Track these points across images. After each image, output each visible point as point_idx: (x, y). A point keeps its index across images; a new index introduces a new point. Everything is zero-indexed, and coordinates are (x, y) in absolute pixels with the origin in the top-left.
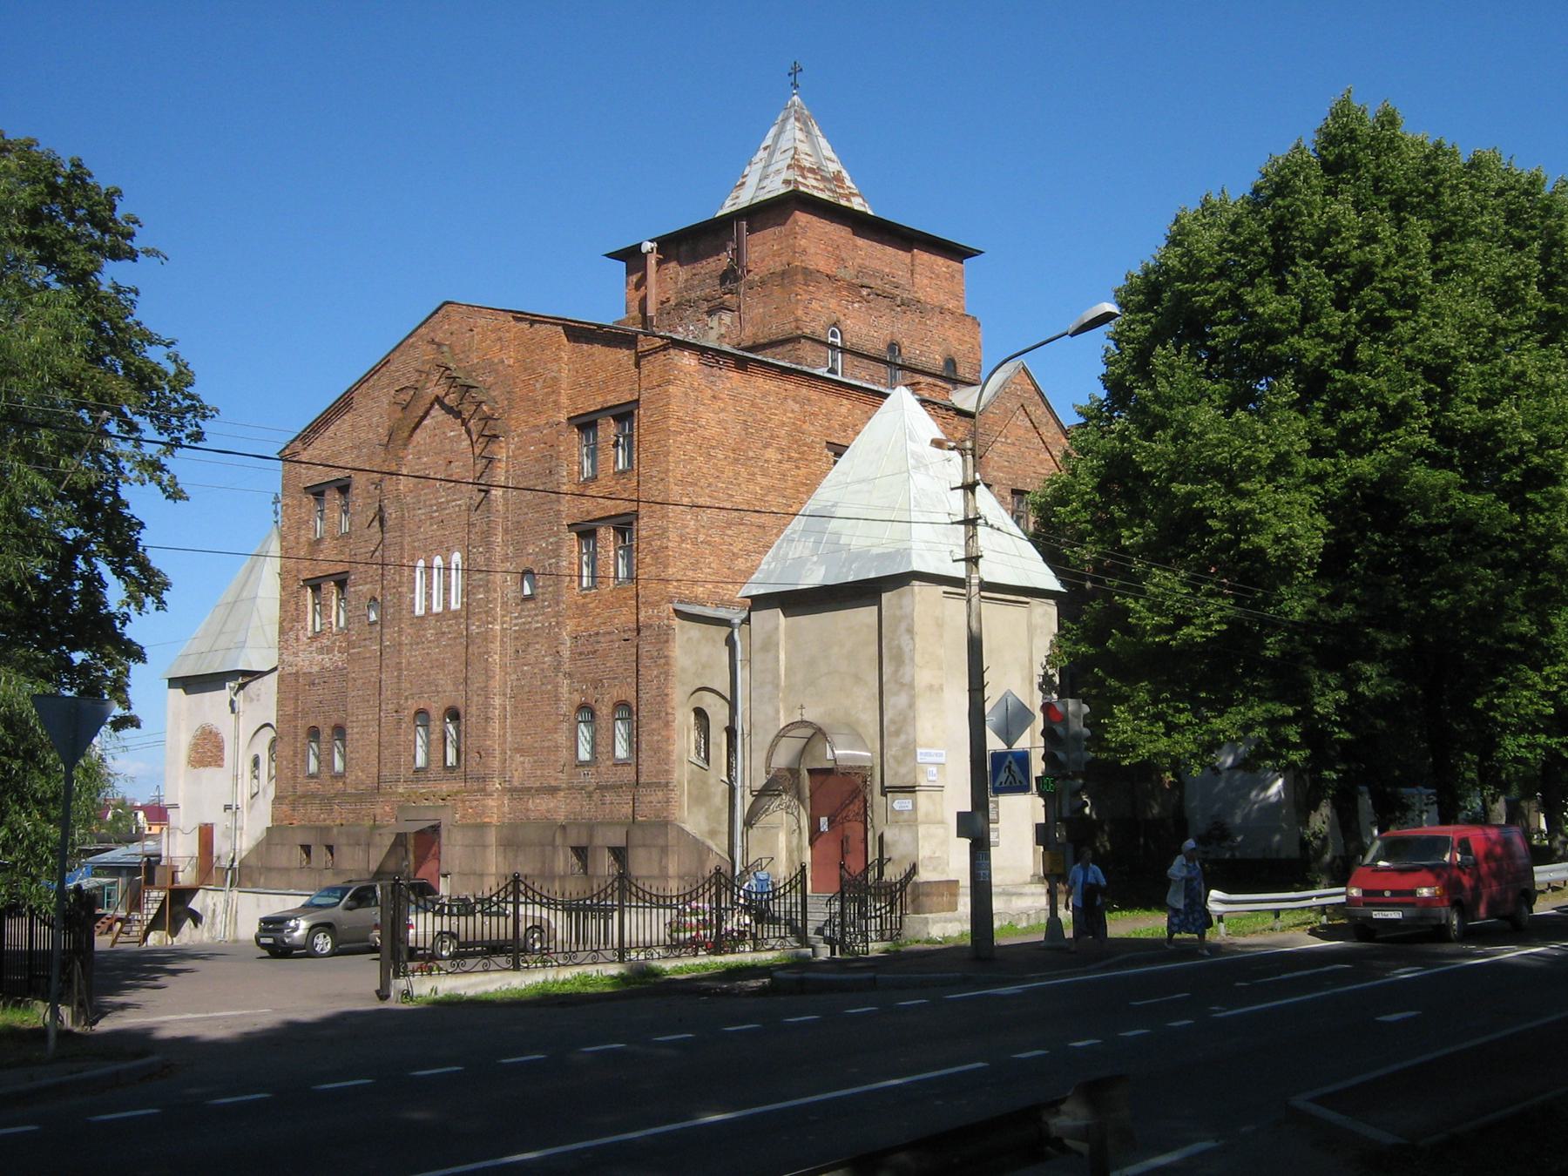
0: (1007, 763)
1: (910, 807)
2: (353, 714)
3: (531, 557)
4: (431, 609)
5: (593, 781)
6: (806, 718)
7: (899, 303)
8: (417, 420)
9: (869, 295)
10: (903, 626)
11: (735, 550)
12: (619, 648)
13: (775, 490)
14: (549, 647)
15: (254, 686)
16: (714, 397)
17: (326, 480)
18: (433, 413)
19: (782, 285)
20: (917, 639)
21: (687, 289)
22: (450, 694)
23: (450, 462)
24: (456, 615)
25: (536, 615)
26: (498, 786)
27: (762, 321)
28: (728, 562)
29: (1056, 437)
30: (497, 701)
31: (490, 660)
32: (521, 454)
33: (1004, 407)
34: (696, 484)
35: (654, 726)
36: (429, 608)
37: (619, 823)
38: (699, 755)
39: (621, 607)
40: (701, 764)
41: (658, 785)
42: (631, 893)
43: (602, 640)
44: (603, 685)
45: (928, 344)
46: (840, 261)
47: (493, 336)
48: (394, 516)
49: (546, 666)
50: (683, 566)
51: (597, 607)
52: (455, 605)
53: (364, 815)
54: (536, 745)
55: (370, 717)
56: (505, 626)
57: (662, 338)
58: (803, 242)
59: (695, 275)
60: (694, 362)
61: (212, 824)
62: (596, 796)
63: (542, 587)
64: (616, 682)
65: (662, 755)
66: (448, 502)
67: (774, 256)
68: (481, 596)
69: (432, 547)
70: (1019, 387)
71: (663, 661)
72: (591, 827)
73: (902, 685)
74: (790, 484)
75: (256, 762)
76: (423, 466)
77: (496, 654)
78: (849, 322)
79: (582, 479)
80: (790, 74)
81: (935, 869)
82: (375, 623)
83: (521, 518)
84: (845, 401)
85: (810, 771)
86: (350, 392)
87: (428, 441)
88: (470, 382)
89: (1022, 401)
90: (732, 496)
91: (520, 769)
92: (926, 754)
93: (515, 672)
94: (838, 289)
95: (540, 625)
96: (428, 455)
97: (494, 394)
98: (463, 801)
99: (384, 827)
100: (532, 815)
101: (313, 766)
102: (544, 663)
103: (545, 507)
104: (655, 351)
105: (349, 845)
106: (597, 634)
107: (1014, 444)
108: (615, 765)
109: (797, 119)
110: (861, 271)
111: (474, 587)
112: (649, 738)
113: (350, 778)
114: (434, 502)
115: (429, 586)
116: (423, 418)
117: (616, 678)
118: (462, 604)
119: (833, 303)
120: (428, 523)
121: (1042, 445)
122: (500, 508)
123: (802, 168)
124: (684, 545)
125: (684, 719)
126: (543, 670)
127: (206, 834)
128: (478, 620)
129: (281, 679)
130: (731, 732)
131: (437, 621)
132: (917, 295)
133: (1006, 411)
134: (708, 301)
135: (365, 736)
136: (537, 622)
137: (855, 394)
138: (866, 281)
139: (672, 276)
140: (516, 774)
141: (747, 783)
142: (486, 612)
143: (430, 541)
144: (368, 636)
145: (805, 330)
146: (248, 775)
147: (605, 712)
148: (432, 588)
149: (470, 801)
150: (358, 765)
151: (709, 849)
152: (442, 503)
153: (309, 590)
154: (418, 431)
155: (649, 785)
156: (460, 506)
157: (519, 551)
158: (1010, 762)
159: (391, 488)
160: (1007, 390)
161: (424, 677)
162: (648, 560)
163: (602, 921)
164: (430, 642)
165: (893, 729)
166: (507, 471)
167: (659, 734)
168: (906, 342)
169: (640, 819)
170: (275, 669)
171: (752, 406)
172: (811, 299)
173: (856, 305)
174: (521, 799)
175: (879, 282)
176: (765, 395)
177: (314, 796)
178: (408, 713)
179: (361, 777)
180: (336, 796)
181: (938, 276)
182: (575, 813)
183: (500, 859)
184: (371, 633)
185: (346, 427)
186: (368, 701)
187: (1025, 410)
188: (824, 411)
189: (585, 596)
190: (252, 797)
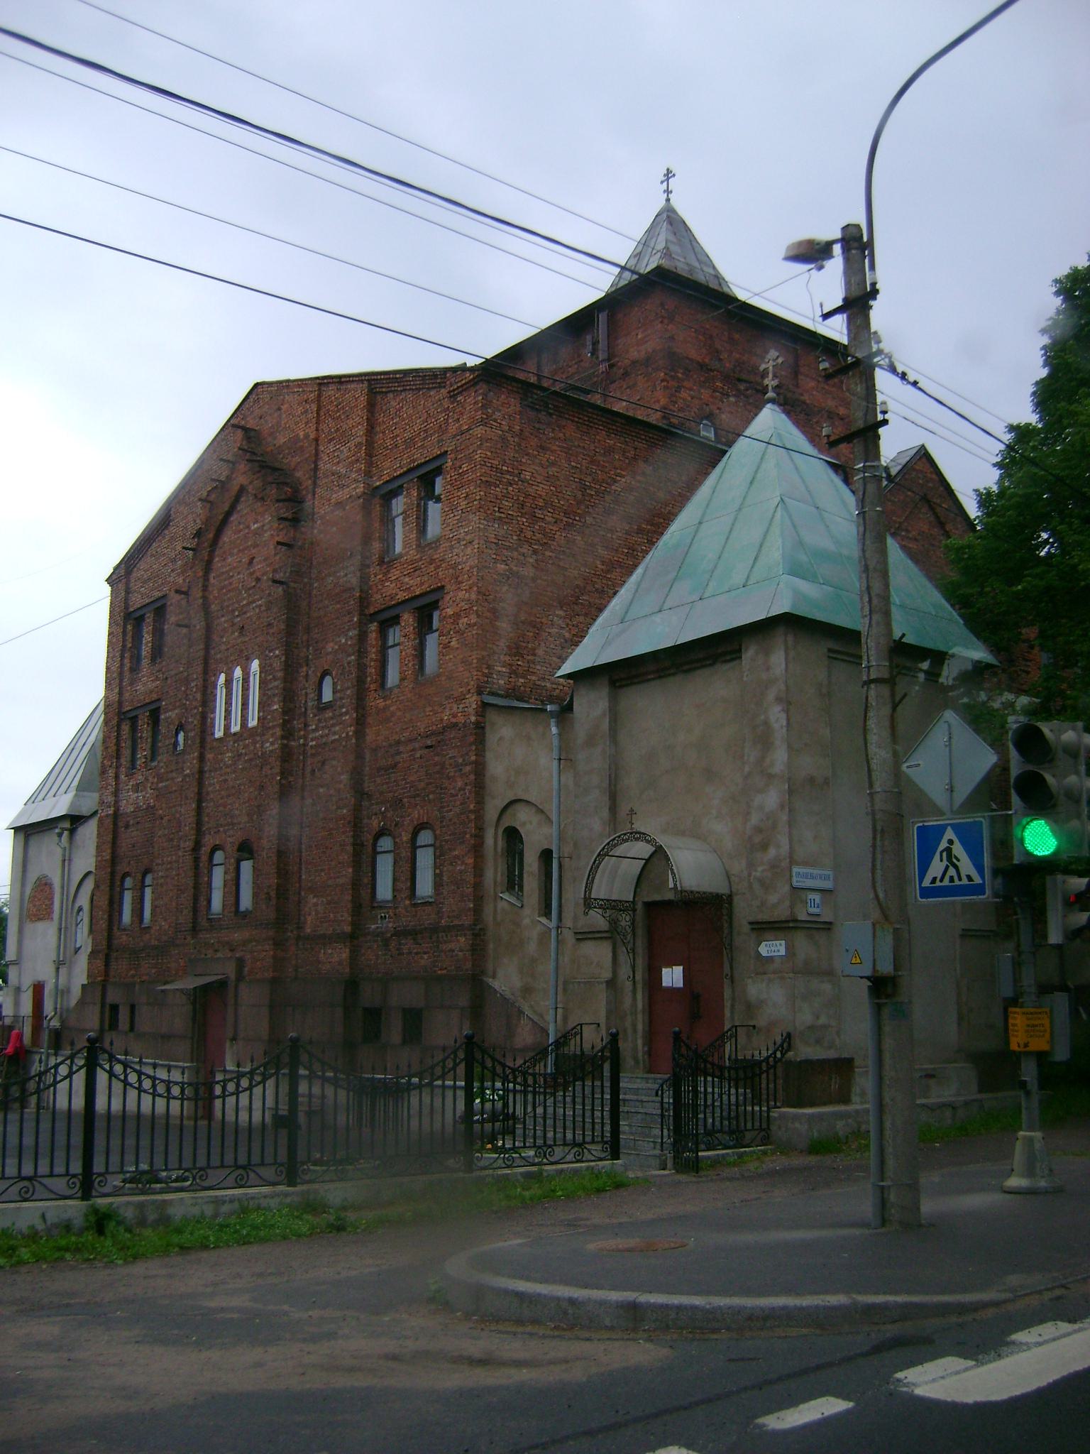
0: (944, 844)
1: (783, 952)
3: (330, 657)
5: (390, 925)
9: (747, 390)
16: (542, 448)
25: (333, 725)
42: (484, 1067)
48: (198, 627)
49: (342, 786)
52: (253, 723)
61: (44, 982)
66: (249, 604)
68: (275, 707)
69: (232, 658)
78: (724, 416)
80: (662, 182)
81: (818, 1042)
90: (565, 569)
92: (806, 876)
95: (337, 737)
107: (916, 540)
112: (451, 868)
117: (418, 795)
119: (705, 393)
127: (38, 989)
129: (101, 821)
136: (335, 733)
138: (744, 376)
140: (309, 919)
144: (173, 768)
147: (405, 839)
151: (521, 1012)
156: (261, 606)
158: (951, 842)
161: (221, 808)
170: (95, 813)
171: (592, 462)
186: (172, 840)
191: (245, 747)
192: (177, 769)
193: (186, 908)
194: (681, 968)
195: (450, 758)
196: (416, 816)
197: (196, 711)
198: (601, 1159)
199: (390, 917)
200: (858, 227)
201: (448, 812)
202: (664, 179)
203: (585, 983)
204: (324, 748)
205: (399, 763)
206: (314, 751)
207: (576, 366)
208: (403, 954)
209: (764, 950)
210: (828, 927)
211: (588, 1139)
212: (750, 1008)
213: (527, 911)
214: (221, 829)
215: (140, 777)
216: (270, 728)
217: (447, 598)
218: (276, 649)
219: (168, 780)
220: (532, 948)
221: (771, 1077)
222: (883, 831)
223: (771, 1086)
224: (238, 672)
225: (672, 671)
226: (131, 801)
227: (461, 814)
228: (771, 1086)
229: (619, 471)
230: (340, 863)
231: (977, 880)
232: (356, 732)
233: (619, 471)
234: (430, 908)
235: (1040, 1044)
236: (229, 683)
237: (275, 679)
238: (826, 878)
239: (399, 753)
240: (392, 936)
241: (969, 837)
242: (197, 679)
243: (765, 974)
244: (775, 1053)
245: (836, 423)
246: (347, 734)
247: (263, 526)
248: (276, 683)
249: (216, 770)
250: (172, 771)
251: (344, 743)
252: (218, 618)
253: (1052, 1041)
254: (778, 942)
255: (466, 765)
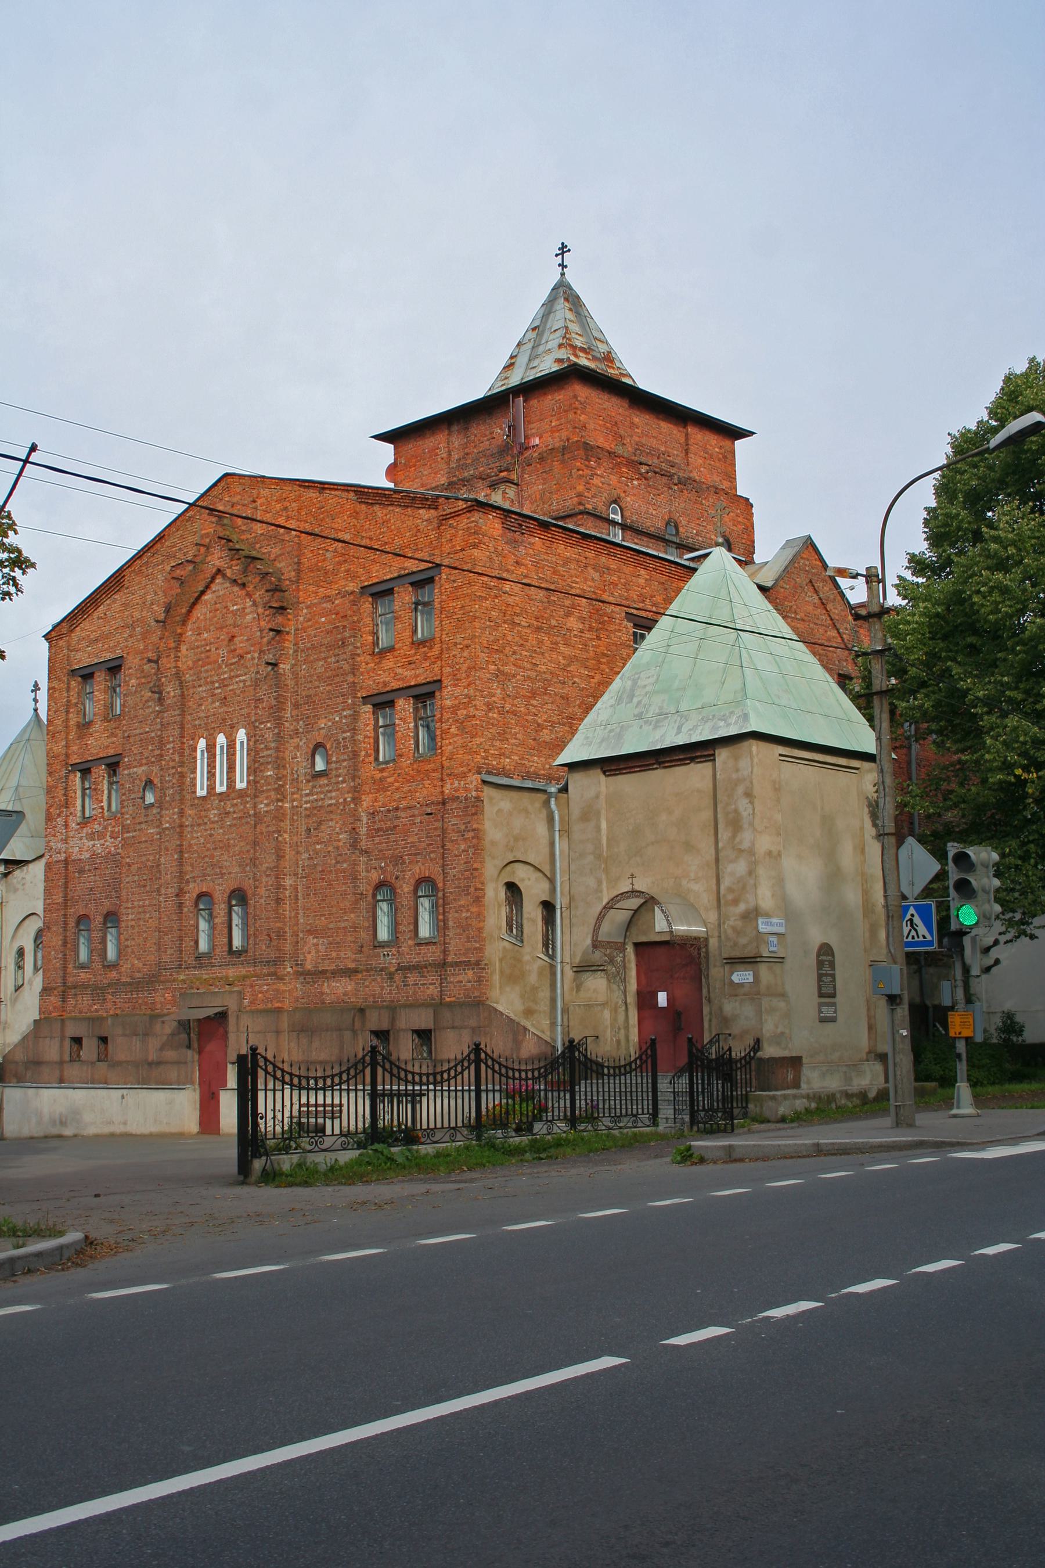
0: (908, 917)
1: (751, 980)
2: (127, 901)
4: (215, 788)
5: (394, 961)
6: (637, 887)
7: (676, 481)
8: (197, 595)
10: (741, 790)
11: (540, 721)
12: (421, 822)
13: (577, 660)
14: (344, 824)
15: (18, 874)
17: (96, 661)
18: (214, 587)
19: (563, 462)
20: (756, 802)
21: (461, 467)
22: (235, 875)
23: (233, 637)
24: (242, 794)
25: (330, 791)
26: (289, 970)
27: (541, 498)
28: (533, 733)
29: (843, 614)
30: (288, 882)
31: (280, 838)
32: (311, 626)
33: (794, 582)
34: (502, 652)
35: (462, 903)
36: (211, 788)
37: (424, 1005)
38: (512, 931)
39: (423, 779)
40: (513, 941)
41: (468, 964)
43: (402, 814)
44: (404, 862)
45: (705, 524)
46: (619, 438)
47: (278, 506)
48: (172, 694)
49: (341, 844)
50: (490, 736)
51: (396, 781)
52: (241, 785)
53: (140, 1005)
54: (331, 926)
55: (147, 902)
56: (295, 804)
57: (466, 500)
58: (583, 417)
59: (467, 454)
60: (498, 525)
62: (397, 977)
63: (336, 762)
64: (419, 858)
65: (476, 935)
66: (231, 678)
67: (552, 432)
68: (269, 773)
69: (213, 725)
70: (807, 563)
71: (471, 834)
72: (393, 1009)
73: (741, 851)
74: (592, 654)
75: (21, 952)
76: (203, 643)
77: (285, 832)
78: (628, 499)
79: (377, 650)
80: (557, 255)
82: (152, 805)
83: (312, 692)
84: (643, 572)
85: (637, 945)
86: (121, 570)
87: (208, 616)
88: (254, 553)
89: (810, 576)
91: (313, 952)
93: (308, 851)
94: (618, 464)
95: (333, 801)
96: (208, 631)
97: (279, 565)
98: (252, 986)
99: (165, 1015)
100: (328, 1000)
101: (83, 955)
102: (339, 841)
103: (337, 679)
104: (456, 515)
105: (124, 1035)
106: (397, 809)
107: (803, 620)
108: (419, 945)
109: (566, 300)
110: (638, 448)
111: (262, 764)
112: (456, 915)
113: (125, 967)
114: (216, 678)
115: (211, 765)
116: (203, 593)
117: (418, 854)
118: (248, 782)
119: (614, 479)
120: (210, 700)
121: (829, 622)
122: (289, 682)
123: (574, 348)
124: (490, 714)
125: (495, 894)
126: (338, 848)
128: (267, 798)
129: (48, 867)
130: (548, 907)
131: (220, 801)
132: (691, 475)
133: (795, 587)
134: (483, 479)
135: (141, 922)
136: (331, 798)
137: (652, 564)
138: (643, 459)
139: (444, 455)
140: (309, 957)
141: (567, 959)
142: (275, 790)
143: (211, 719)
144: (142, 819)
145: (587, 506)
146: (12, 967)
147: (406, 890)
148: (215, 767)
149: (261, 986)
150: (133, 952)
152: (225, 679)
153: (79, 774)
154: (198, 607)
155: (457, 964)
156: (244, 681)
157: (310, 727)
158: (912, 915)
159: (168, 666)
160: (796, 565)
161: (207, 860)
162: (453, 730)
163: (409, 1106)
164: (213, 822)
165: (730, 897)
166: (296, 644)
167: (468, 910)
168: (683, 521)
169: (448, 999)
172: (592, 475)
173: (635, 482)
174: (314, 982)
175: (656, 461)
176: (567, 561)
177: (85, 986)
178: (189, 899)
179: (135, 966)
180: (110, 985)
181: (711, 457)
182: (374, 996)
183: (292, 1044)
184: (147, 816)
185: (116, 606)
186: (145, 886)
187: (813, 586)
188: (622, 581)
189: (382, 770)
190: (16, 991)
191: (234, 805)
192: (146, 822)
193: (171, 948)
194: (665, 993)
195: (453, 825)
196: (418, 871)
197: (174, 771)
198: (648, 1126)
199: (393, 955)
200: (876, 568)
201: (451, 869)
202: (559, 252)
203: (584, 1005)
204: (319, 811)
205: (399, 826)
206: (308, 813)
207: (488, 443)
208: (409, 985)
209: (736, 978)
210: (781, 960)
211: (640, 1111)
212: (725, 1021)
213: (527, 949)
214: (209, 878)
215: (96, 827)
216: (263, 791)
217: (445, 692)
218: (268, 722)
219: (135, 831)
220: (533, 979)
221: (748, 1071)
222: (893, 916)
223: (748, 1076)
224: (221, 739)
225: (655, 766)
226: (85, 848)
227: (465, 871)
228: (748, 1076)
229: (574, 579)
230: (341, 909)
231: (929, 938)
232: (354, 799)
233: (574, 579)
234: (434, 947)
235: (967, 1033)
236: (211, 747)
237: (267, 748)
238: (781, 925)
239: (397, 818)
240: (397, 970)
241: (924, 913)
242: (173, 742)
243: (736, 996)
244: (749, 1053)
245: (722, 498)
246: (345, 800)
247: (244, 609)
248: (269, 752)
249: (199, 825)
250: (140, 823)
251: (341, 807)
252: (194, 687)
253: (974, 1031)
254: (747, 973)
255: (469, 831)
